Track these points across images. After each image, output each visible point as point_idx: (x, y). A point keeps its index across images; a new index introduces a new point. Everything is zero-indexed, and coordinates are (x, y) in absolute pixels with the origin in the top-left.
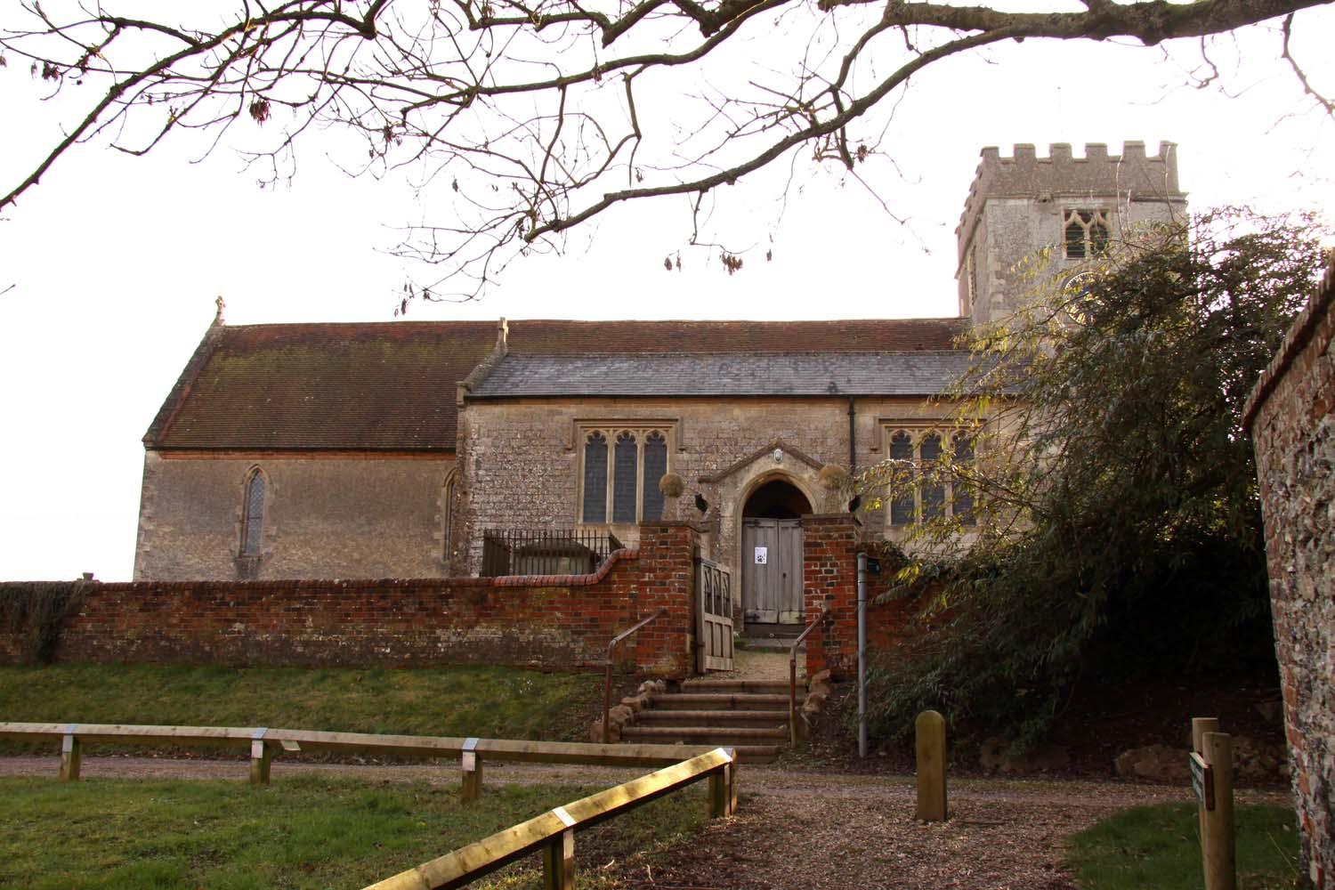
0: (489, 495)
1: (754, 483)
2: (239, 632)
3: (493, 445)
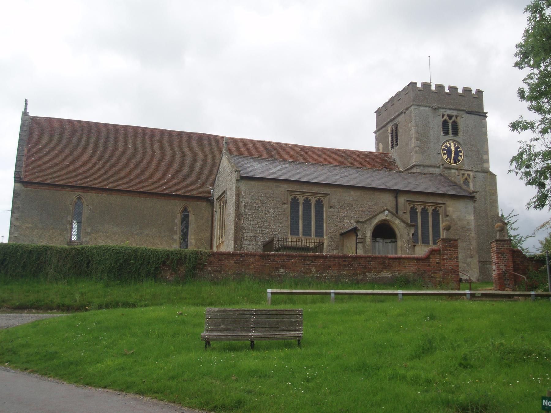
0: (250, 221)
1: (377, 223)
2: (282, 272)
3: (252, 199)
